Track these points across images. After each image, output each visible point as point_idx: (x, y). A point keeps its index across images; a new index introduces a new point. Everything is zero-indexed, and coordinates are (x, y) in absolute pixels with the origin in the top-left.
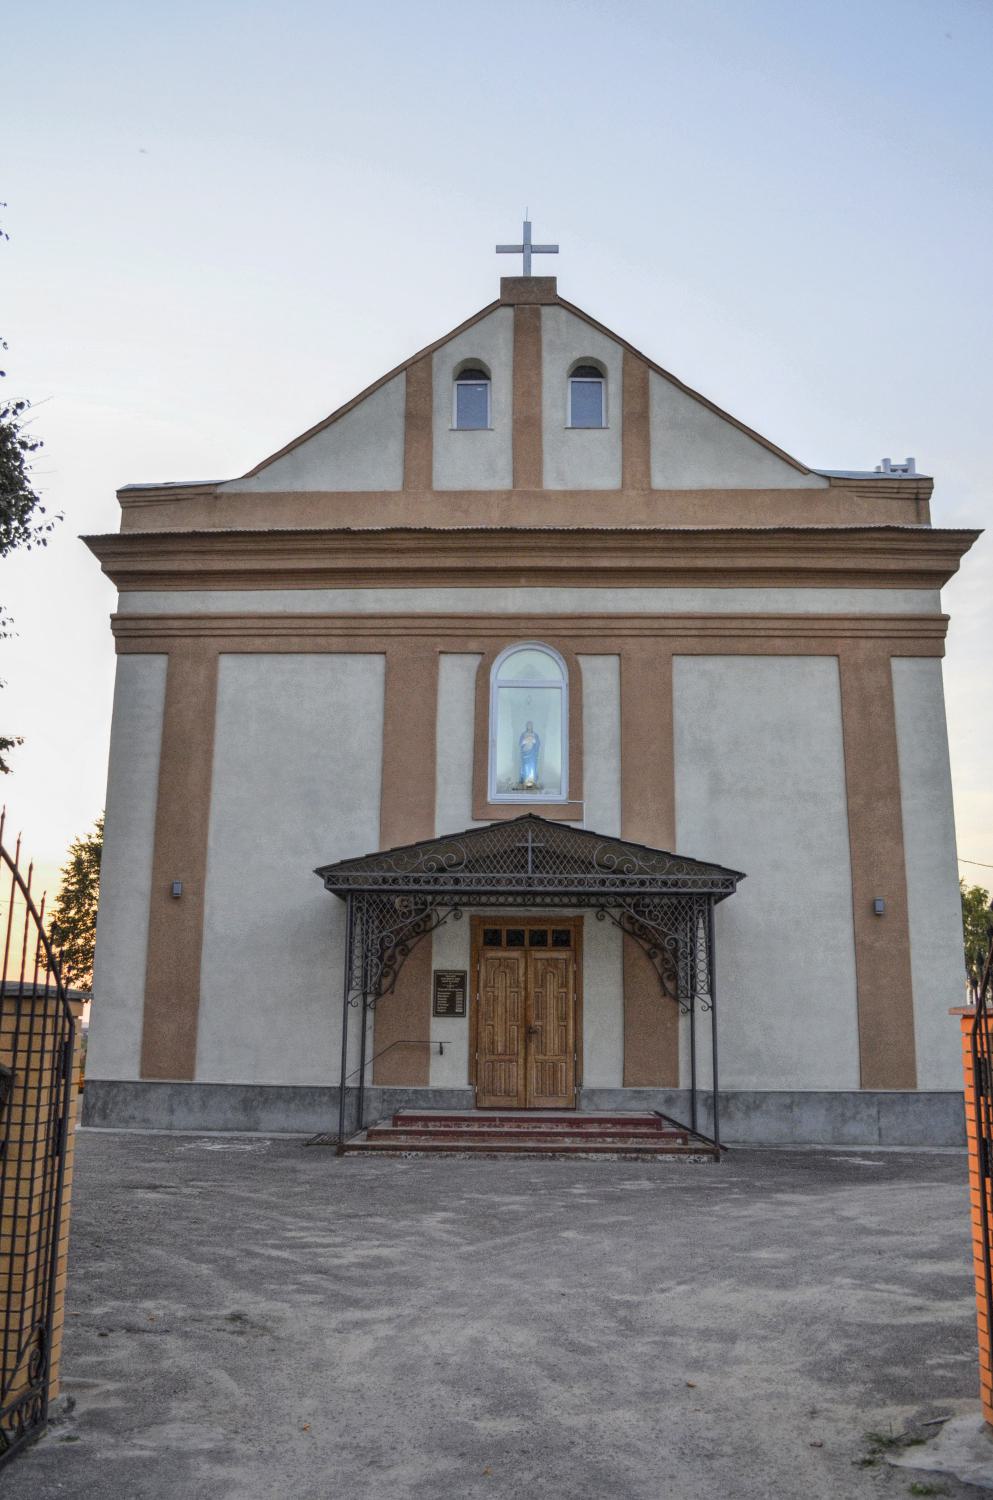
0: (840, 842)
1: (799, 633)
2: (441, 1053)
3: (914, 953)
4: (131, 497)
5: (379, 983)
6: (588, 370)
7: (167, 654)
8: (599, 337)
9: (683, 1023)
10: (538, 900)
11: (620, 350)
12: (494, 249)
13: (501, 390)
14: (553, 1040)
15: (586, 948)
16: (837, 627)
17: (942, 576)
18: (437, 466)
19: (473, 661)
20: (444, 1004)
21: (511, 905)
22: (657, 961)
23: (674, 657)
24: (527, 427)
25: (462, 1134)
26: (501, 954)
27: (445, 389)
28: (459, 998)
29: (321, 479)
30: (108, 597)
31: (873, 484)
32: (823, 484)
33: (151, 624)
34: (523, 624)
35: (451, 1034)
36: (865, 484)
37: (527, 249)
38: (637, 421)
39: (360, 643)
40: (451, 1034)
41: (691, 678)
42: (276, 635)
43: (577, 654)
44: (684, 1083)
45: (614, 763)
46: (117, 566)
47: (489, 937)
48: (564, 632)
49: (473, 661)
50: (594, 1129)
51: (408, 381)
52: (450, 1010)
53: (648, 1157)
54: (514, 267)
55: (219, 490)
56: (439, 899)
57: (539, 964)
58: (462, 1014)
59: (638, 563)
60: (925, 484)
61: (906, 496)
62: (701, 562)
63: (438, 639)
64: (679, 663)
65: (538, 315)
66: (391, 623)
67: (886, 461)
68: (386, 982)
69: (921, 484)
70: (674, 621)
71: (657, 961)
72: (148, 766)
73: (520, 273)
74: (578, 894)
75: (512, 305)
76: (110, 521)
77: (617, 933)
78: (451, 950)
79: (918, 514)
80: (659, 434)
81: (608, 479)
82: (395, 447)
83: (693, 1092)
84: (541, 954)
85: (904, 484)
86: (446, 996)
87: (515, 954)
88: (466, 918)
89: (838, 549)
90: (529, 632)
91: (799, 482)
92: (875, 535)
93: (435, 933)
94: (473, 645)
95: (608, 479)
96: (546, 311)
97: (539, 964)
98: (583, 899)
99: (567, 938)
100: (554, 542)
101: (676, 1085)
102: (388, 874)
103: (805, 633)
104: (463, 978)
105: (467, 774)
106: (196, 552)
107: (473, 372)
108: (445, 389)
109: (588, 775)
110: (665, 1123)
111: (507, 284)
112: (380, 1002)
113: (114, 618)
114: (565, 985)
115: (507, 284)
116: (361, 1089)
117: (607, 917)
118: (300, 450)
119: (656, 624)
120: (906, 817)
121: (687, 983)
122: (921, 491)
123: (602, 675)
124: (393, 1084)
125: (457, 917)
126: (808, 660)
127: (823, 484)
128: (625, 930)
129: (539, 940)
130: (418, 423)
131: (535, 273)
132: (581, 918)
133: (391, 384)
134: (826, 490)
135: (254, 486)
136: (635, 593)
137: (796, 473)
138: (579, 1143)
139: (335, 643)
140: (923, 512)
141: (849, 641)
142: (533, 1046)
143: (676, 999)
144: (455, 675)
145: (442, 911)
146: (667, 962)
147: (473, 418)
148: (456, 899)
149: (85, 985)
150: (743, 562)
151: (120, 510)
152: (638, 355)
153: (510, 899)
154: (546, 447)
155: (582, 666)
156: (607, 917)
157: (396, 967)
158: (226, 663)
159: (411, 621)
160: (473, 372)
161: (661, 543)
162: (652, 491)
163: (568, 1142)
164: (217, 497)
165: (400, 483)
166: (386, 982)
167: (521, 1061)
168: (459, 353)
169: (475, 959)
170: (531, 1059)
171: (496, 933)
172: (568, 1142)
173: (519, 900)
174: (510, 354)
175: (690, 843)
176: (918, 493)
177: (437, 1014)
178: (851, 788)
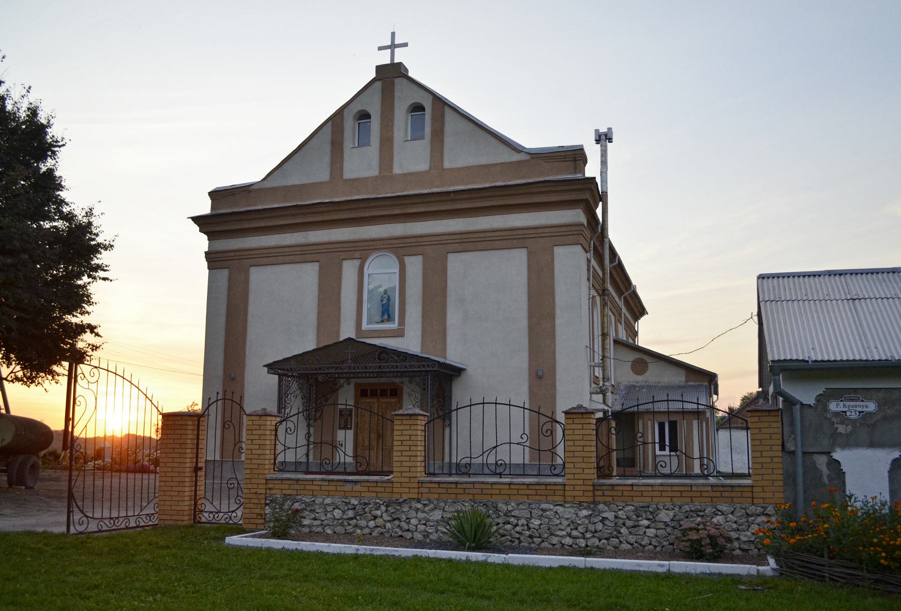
0: (525, 342)
1: (506, 238)
3: (558, 397)
4: (215, 195)
5: (315, 414)
6: (418, 108)
7: (318, 261)
8: (422, 92)
9: (447, 431)
10: (360, 375)
11: (431, 97)
13: (375, 124)
16: (526, 233)
18: (345, 165)
19: (357, 263)
20: (343, 423)
21: (371, 377)
22: (412, 398)
23: (449, 254)
24: (387, 143)
26: (368, 400)
27: (350, 125)
28: (349, 420)
29: (294, 180)
30: (202, 242)
31: (551, 155)
32: (528, 157)
33: (221, 255)
34: (378, 243)
35: (345, 437)
36: (548, 155)
37: (393, 47)
38: (438, 135)
39: (309, 257)
40: (345, 437)
41: (456, 263)
42: (282, 256)
43: (403, 256)
44: (447, 460)
45: (420, 308)
46: (206, 230)
47: (363, 392)
48: (397, 246)
49: (357, 263)
51: (333, 126)
52: (345, 427)
54: (384, 58)
55: (251, 188)
56: (340, 376)
57: (384, 405)
58: (351, 428)
59: (429, 209)
60: (579, 152)
61: (568, 159)
62: (458, 206)
63: (342, 253)
64: (451, 257)
65: (393, 84)
66: (320, 247)
67: (89, 213)
68: (318, 414)
70: (559, 228)
71: (412, 398)
72: (222, 320)
74: (377, 372)
75: (381, 80)
76: (205, 208)
78: (346, 397)
80: (448, 140)
81: (423, 166)
82: (327, 159)
83: (450, 463)
85: (567, 153)
86: (343, 420)
87: (374, 400)
88: (352, 386)
89: (487, 197)
90: (382, 247)
91: (516, 157)
92: (542, 185)
93: (340, 391)
94: (357, 255)
95: (423, 166)
96: (397, 81)
97: (384, 405)
98: (403, 374)
99: (395, 392)
100: (389, 202)
102: (312, 366)
103: (510, 237)
104: (351, 411)
105: (354, 317)
106: (237, 221)
107: (364, 116)
108: (350, 125)
109: (408, 314)
111: (379, 69)
113: (206, 253)
115: (379, 69)
116: (308, 462)
117: (414, 382)
118: (285, 166)
119: (438, 238)
120: (558, 328)
121: (796, 445)
122: (577, 156)
123: (415, 265)
125: (349, 384)
126: (513, 250)
127: (528, 157)
129: (384, 393)
130: (337, 147)
131: (395, 62)
133: (325, 128)
134: (529, 160)
135: (267, 185)
136: (445, 222)
137: (514, 152)
139: (298, 258)
141: (532, 239)
144: (349, 269)
145: (342, 381)
146: (440, 402)
147: (363, 141)
148: (348, 375)
150: (478, 204)
151: (210, 201)
153: (371, 375)
154: (395, 152)
156: (414, 382)
157: (292, 404)
159: (329, 245)
160: (364, 116)
161: (438, 199)
162: (443, 170)
164: (250, 192)
165: (329, 176)
166: (318, 414)
168: (357, 107)
169: (356, 402)
171: (391, 395)
173: (375, 375)
174: (380, 105)
175: (453, 357)
176: (575, 157)
177: (340, 428)
178: (531, 315)
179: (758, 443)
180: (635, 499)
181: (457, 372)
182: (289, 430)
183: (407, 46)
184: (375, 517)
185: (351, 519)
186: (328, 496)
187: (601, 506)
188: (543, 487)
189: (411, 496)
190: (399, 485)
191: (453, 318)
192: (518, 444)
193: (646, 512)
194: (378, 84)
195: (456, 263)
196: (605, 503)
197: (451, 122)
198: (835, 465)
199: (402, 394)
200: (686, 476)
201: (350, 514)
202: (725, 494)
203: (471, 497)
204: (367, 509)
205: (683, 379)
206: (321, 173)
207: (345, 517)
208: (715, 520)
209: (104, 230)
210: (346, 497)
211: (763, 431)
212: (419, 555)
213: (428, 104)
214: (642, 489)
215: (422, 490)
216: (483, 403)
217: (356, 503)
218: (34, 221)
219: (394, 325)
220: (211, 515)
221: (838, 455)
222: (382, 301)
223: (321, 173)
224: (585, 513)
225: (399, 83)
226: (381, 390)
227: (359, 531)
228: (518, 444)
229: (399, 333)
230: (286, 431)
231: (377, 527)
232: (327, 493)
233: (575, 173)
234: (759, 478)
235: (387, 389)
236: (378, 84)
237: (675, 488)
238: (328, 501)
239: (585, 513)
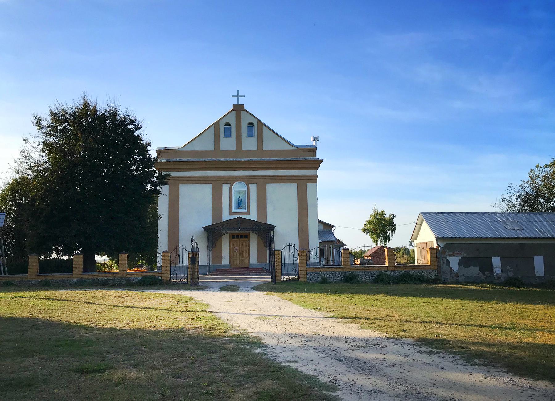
2: (224, 258)
6: (251, 124)
12: (320, 139)
14: (244, 255)
15: (251, 239)
17: (317, 168)
19: (229, 185)
25: (228, 271)
32: (296, 149)
37: (238, 96)
41: (271, 188)
49: (229, 185)
50: (252, 270)
53: (260, 274)
55: (177, 150)
69: (314, 149)
73: (237, 103)
77: (256, 235)
79: (314, 154)
81: (255, 148)
84: (242, 240)
87: (238, 240)
88: (228, 234)
91: (292, 148)
94: (229, 182)
99: (247, 237)
101: (267, 262)
108: (222, 129)
110: (263, 268)
112: (213, 249)
114: (246, 245)
118: (193, 142)
123: (253, 188)
124: (287, 157)
127: (296, 149)
128: (257, 235)
129: (242, 237)
132: (249, 233)
133: (211, 128)
135: (184, 149)
138: (249, 272)
140: (315, 155)
142: (241, 257)
143: (267, 247)
144: (225, 188)
149: (130, 269)
152: (261, 122)
155: (250, 186)
158: (180, 186)
163: (247, 272)
167: (239, 259)
170: (240, 259)
172: (247, 272)
175: (270, 221)
181: (272, 227)
184: (338, 277)
185: (332, 277)
186: (325, 272)
187: (396, 272)
189: (348, 270)
191: (269, 209)
194: (234, 112)
195: (271, 188)
196: (397, 271)
197: (265, 131)
198: (448, 260)
199: (249, 237)
200: (329, 265)
201: (332, 276)
202: (424, 268)
203: (364, 270)
204: (336, 275)
205: (322, 228)
206: (210, 147)
207: (330, 277)
208: (422, 274)
213: (255, 123)
215: (351, 269)
217: (333, 273)
218: (125, 170)
219: (246, 211)
220: (287, 279)
221: (448, 258)
222: (238, 200)
223: (210, 147)
224: (393, 273)
225: (243, 114)
226: (236, 236)
227: (334, 281)
229: (248, 213)
231: (339, 279)
233: (314, 156)
235: (243, 236)
236: (234, 112)
238: (325, 273)
239: (393, 273)
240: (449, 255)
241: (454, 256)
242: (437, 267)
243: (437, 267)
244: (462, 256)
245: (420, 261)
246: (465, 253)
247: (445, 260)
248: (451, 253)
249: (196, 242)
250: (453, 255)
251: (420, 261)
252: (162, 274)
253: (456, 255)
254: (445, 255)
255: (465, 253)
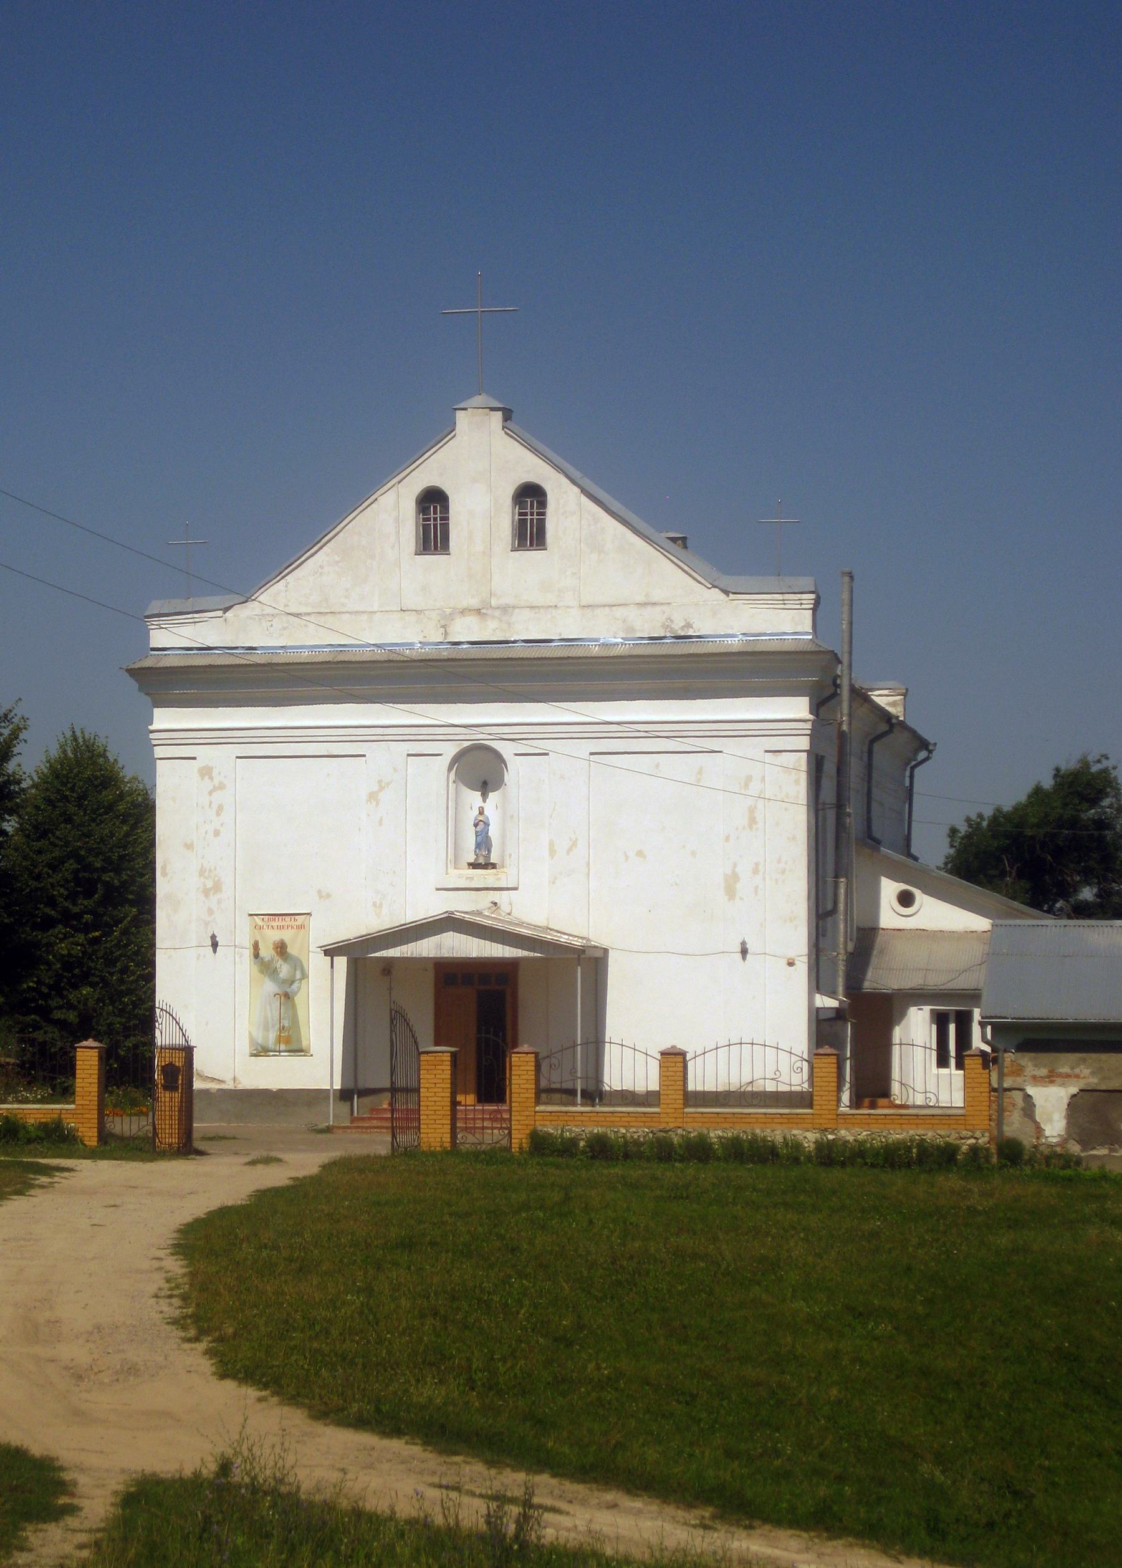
49: (151, 631)
158: (808, 698)
179: (970, 1080)
180: (871, 1126)
182: (553, 1067)
183: (823, 757)
188: (595, 1114)
190: (426, 1108)
192: (772, 1079)
193: (879, 1136)
198: (1028, 1098)
209: (1068, 763)
210: (614, 1127)
211: (437, 1076)
212: (372, 1155)
214: (693, 1115)
216: (741, 1044)
221: (1030, 1090)
228: (772, 1079)
230: (551, 1066)
232: (596, 1123)
234: (970, 1108)
237: (767, 1116)
240: (1037, 1080)
241: (1052, 1082)
242: (990, 1120)
243: (510, 1120)
244: (1083, 1084)
245: (932, 1096)
246: (1093, 1073)
247: (1017, 1096)
248: (1044, 1072)
249: (405, 1020)
250: (1051, 1078)
251: (932, 1096)
252: (810, 1121)
253: (1058, 1080)
254: (1019, 1080)
255: (1093, 1073)
